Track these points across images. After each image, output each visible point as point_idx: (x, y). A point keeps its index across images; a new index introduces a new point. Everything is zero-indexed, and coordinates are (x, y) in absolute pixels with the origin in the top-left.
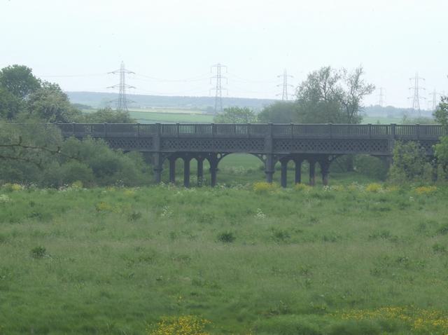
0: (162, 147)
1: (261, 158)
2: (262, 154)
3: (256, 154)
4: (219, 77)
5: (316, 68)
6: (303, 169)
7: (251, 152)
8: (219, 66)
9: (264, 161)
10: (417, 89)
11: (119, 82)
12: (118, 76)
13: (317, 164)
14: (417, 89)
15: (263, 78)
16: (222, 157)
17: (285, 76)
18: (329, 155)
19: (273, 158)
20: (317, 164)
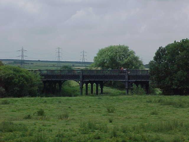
0: (129, 79)
1: (78, 82)
2: (79, 81)
3: (77, 81)
4: (59, 52)
5: (128, 46)
6: (88, 86)
7: (75, 80)
8: (59, 48)
9: (79, 83)
10: (84, 55)
11: (21, 55)
12: (21, 52)
13: (99, 84)
14: (84, 55)
15: (82, 51)
16: (63, 82)
17: (83, 52)
18: (62, 81)
19: (83, 83)
20: (99, 84)
